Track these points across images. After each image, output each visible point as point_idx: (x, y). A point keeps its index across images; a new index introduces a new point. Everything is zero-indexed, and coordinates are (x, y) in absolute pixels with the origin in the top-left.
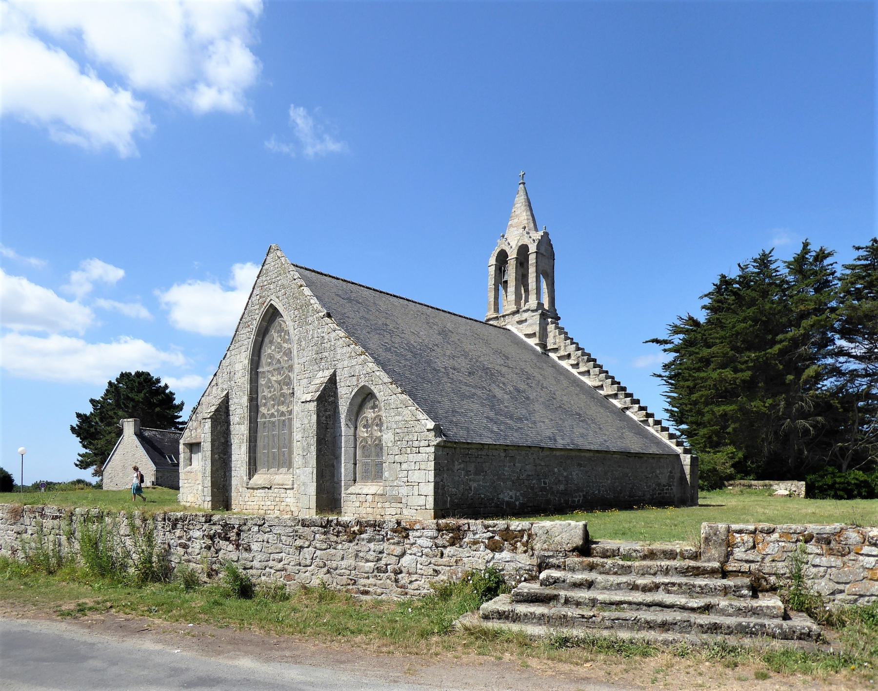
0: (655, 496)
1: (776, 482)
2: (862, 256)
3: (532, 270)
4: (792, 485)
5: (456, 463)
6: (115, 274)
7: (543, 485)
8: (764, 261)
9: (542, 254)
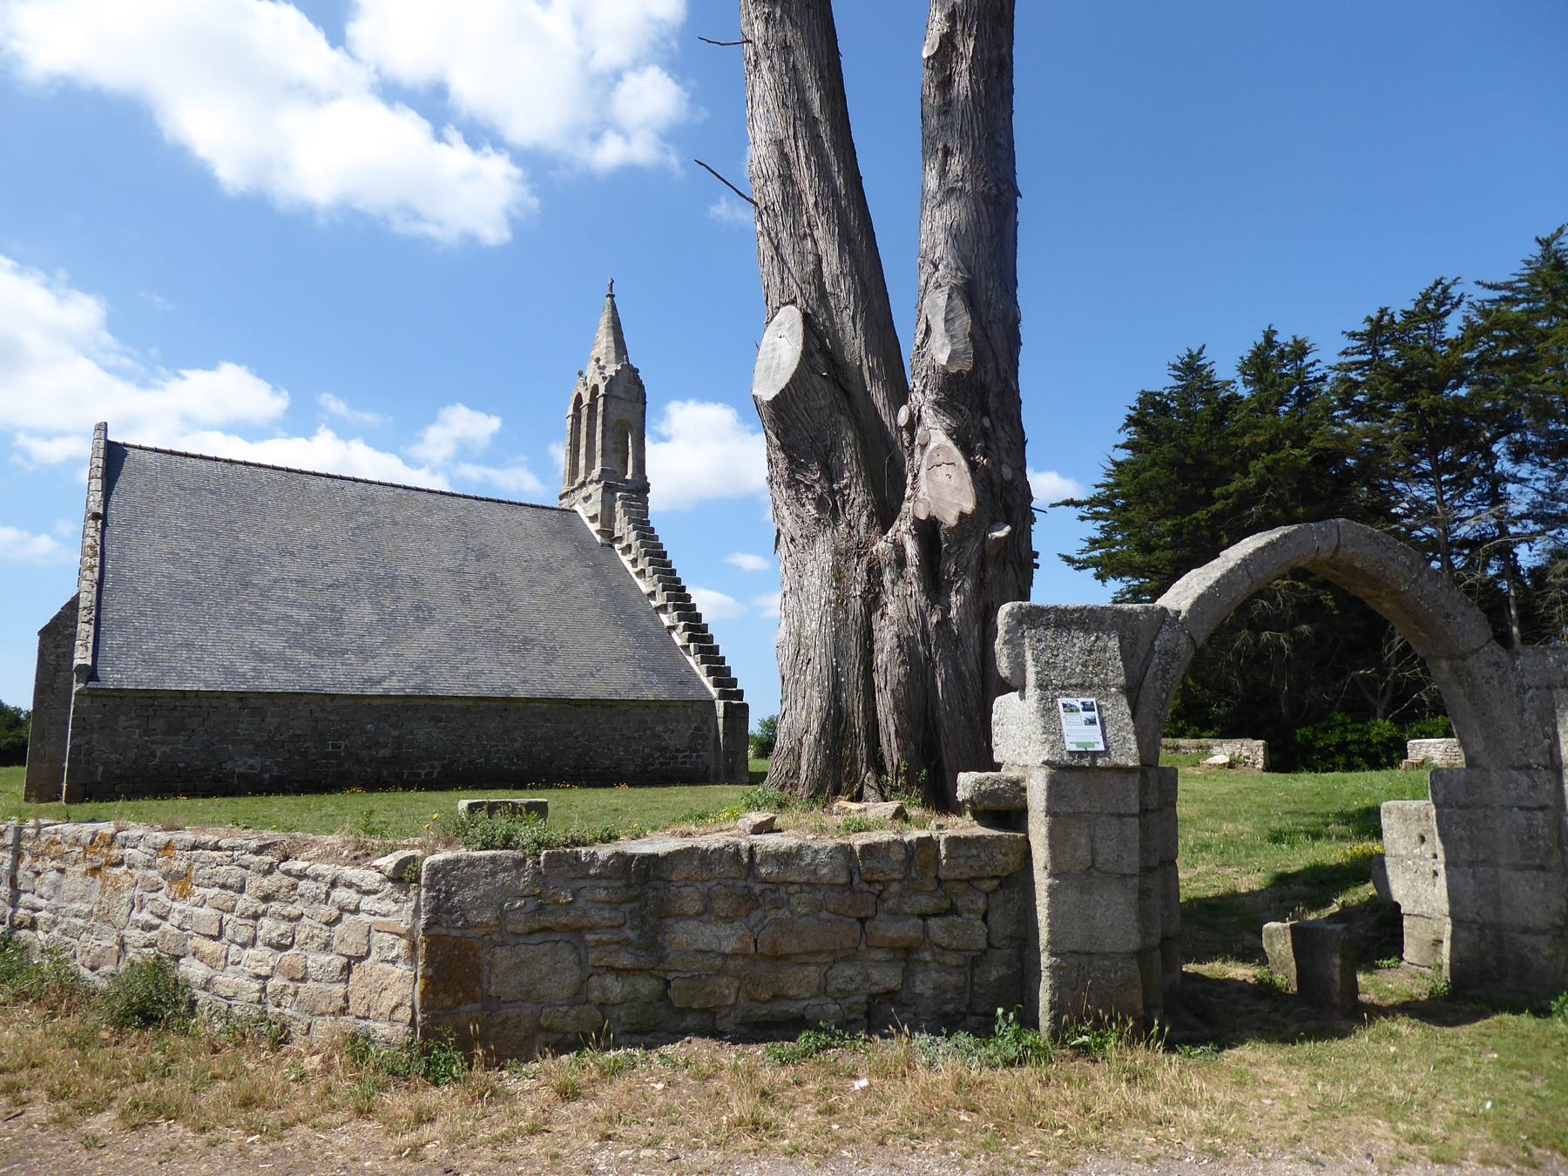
0: (650, 768)
1: (1218, 741)
2: (1353, 348)
4: (1242, 745)
6: (484, 426)
8: (1191, 368)
9: (617, 397)
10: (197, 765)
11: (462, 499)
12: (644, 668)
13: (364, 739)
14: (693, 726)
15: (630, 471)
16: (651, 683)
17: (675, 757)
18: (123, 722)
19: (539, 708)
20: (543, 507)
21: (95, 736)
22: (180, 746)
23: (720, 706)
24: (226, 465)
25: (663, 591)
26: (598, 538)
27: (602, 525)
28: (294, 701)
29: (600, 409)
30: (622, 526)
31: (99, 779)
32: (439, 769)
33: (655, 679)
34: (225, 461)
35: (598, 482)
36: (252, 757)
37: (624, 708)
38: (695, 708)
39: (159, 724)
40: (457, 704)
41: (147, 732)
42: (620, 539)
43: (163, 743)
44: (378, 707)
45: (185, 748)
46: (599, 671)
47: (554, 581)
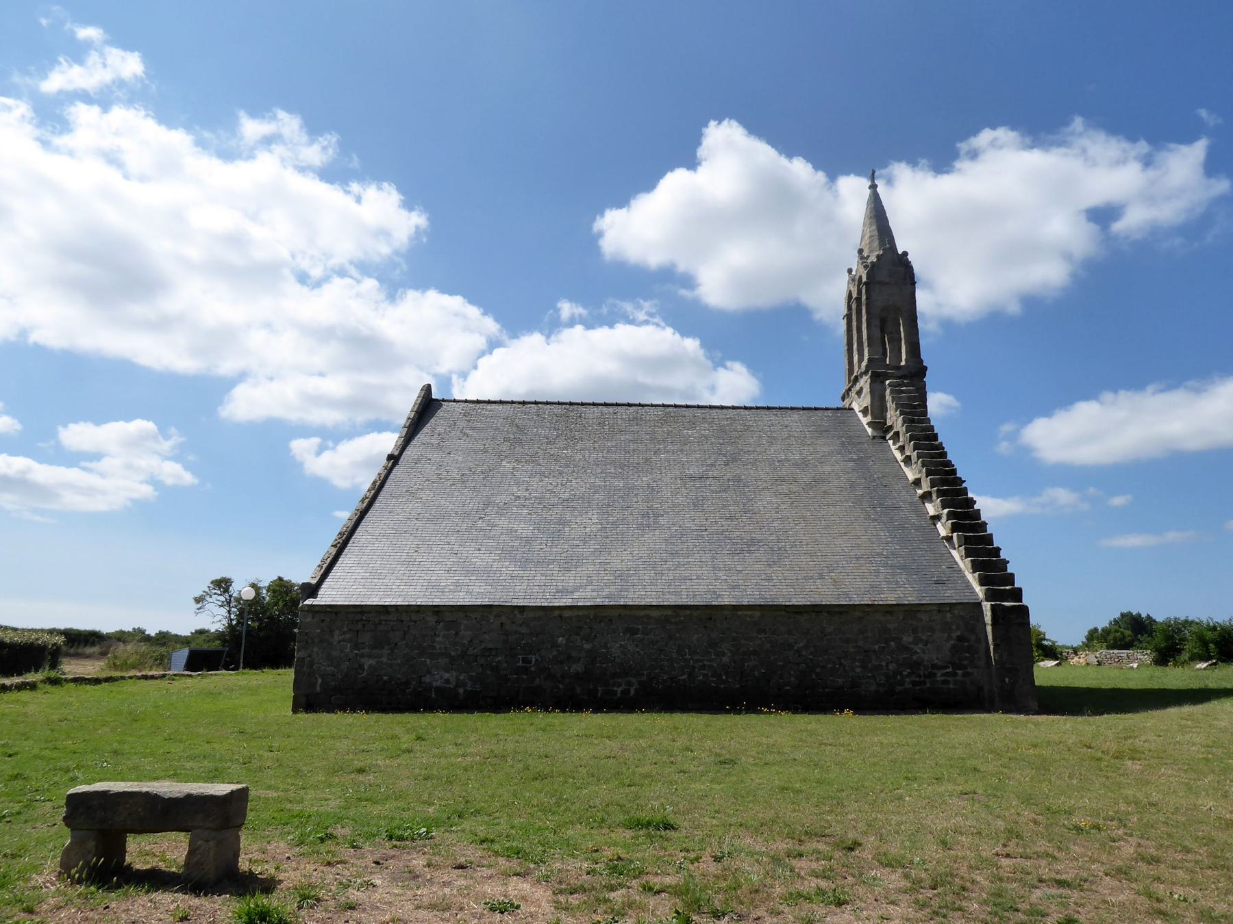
0: (899, 688)
3: (866, 344)
5: (337, 632)
7: (520, 663)
10: (399, 679)
11: (731, 410)
12: (891, 566)
13: (555, 653)
14: (954, 635)
15: (904, 357)
16: (897, 583)
17: (933, 675)
18: (337, 636)
19: (751, 616)
20: (816, 409)
21: (315, 649)
22: (384, 660)
23: (987, 607)
24: (520, 406)
25: (927, 477)
26: (869, 430)
27: (873, 417)
28: (485, 614)
29: (864, 297)
30: (894, 418)
31: (318, 689)
32: (636, 686)
33: (903, 578)
34: (519, 403)
35: (865, 373)
36: (447, 671)
37: (857, 614)
38: (956, 612)
39: (366, 638)
40: (655, 614)
41: (356, 646)
42: (891, 427)
43: (370, 656)
44: (570, 618)
45: (389, 662)
46: (831, 571)
47: (805, 478)
